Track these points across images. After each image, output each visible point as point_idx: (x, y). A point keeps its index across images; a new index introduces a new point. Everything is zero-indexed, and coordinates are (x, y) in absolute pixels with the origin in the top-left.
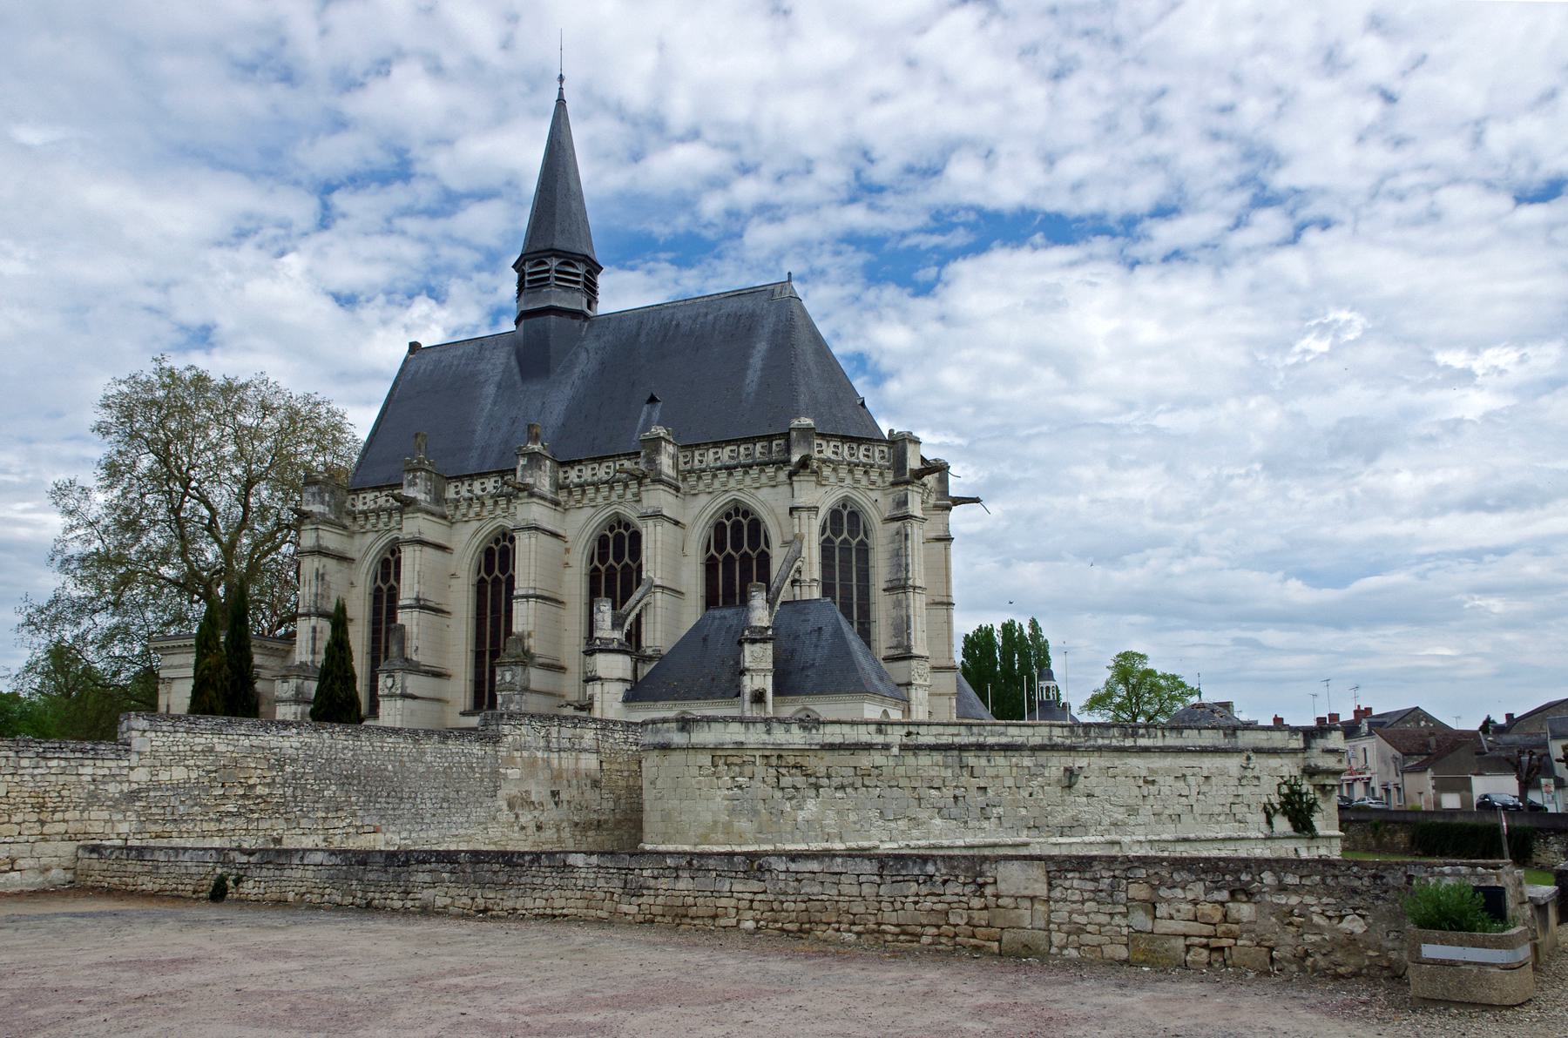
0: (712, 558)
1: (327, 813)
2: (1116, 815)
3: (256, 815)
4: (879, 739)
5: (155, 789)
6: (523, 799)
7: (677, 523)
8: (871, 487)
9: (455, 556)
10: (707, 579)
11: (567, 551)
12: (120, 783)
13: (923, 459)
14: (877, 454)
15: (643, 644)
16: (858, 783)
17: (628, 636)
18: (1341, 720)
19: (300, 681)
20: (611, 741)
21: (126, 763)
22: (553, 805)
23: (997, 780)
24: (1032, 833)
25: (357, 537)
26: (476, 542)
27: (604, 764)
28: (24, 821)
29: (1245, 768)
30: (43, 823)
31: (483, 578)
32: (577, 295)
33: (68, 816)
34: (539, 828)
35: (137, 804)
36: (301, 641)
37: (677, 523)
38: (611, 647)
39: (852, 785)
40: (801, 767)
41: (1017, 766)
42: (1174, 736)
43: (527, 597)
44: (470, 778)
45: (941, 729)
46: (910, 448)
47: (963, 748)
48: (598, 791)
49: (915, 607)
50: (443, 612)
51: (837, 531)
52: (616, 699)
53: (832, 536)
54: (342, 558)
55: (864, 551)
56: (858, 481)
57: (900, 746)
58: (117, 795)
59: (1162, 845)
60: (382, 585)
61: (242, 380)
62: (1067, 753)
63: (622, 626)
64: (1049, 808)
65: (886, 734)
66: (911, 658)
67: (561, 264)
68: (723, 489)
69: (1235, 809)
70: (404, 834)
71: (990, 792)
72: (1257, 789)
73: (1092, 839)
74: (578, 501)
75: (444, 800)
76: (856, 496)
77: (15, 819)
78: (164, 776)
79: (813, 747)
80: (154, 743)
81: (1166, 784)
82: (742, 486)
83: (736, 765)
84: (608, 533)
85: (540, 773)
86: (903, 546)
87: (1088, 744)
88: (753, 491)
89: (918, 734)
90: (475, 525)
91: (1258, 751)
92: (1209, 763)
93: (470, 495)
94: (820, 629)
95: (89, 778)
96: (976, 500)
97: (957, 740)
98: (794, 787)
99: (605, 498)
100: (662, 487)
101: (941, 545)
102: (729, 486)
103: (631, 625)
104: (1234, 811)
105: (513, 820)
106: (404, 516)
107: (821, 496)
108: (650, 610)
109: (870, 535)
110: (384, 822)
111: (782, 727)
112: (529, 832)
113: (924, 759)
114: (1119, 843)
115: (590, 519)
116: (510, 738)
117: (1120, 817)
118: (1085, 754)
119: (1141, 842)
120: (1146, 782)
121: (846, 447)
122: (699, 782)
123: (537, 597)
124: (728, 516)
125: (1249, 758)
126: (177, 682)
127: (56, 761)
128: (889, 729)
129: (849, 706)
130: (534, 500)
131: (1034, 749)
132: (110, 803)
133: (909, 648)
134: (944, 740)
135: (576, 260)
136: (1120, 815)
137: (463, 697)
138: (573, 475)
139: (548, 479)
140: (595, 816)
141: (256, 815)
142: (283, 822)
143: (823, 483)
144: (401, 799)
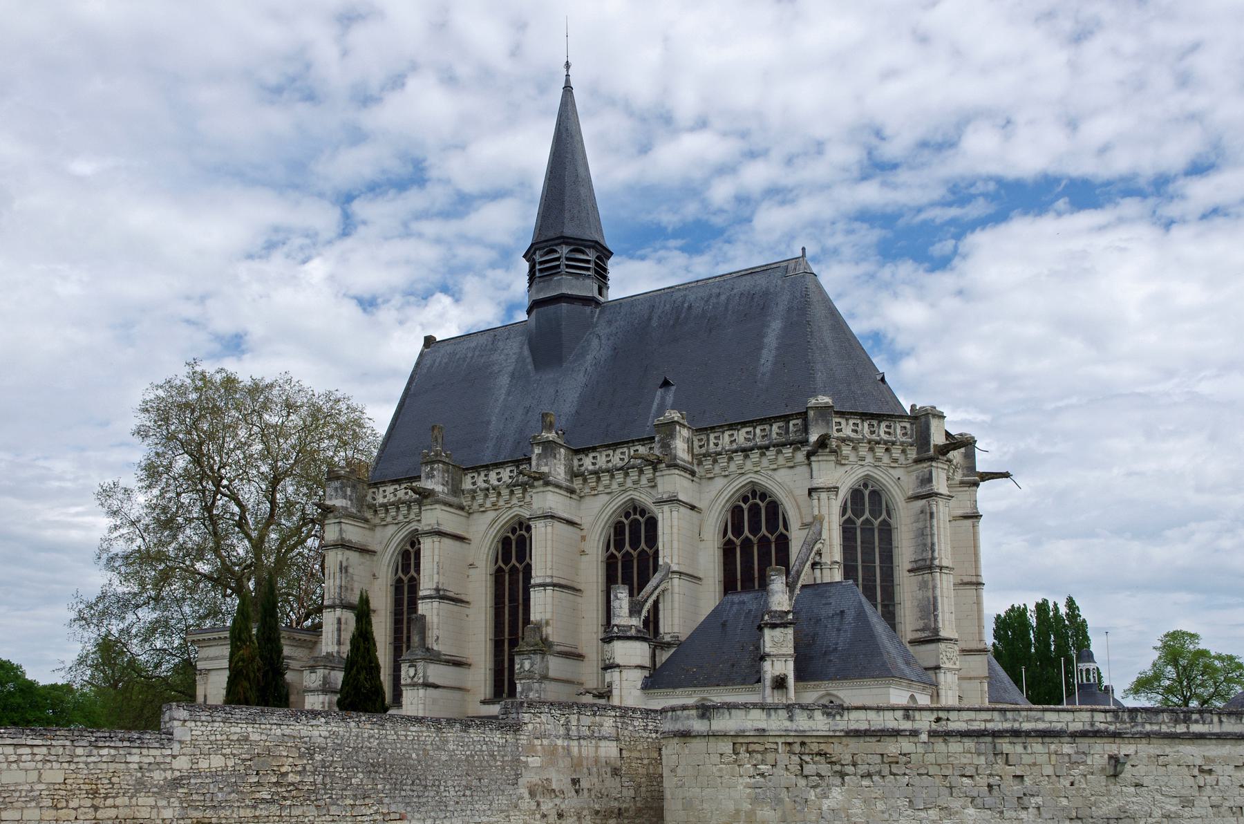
0: (729, 542)
1: (355, 801)
2: (1168, 807)
3: (289, 802)
4: (907, 725)
5: (195, 777)
6: (544, 787)
7: (693, 508)
8: (893, 465)
10: (725, 564)
11: (583, 538)
12: (165, 770)
13: (948, 435)
14: (898, 431)
15: (661, 630)
16: (886, 771)
17: (646, 623)
19: (327, 671)
21: (169, 752)
22: (573, 793)
26: (493, 532)
27: (624, 752)
28: (79, 807)
30: (96, 808)
31: (500, 567)
32: (588, 281)
33: (119, 801)
35: (180, 790)
37: (693, 508)
38: (629, 634)
39: (879, 773)
40: (825, 754)
42: (1233, 721)
43: (544, 585)
45: (972, 715)
46: (934, 423)
47: (996, 734)
48: (618, 779)
49: (942, 588)
50: (462, 601)
51: (858, 512)
52: (635, 687)
54: (364, 551)
55: (887, 531)
57: (929, 732)
58: (162, 782)
60: (503, 566)
61: (268, 381)
62: (1111, 740)
63: (640, 612)
64: (1093, 799)
65: (914, 720)
66: (939, 640)
67: (571, 251)
71: (1028, 781)
74: (593, 489)
75: (466, 787)
76: (878, 474)
77: (72, 805)
78: (203, 764)
79: (838, 734)
83: (758, 752)
84: (623, 519)
85: (560, 762)
86: (928, 525)
89: (948, 719)
90: (491, 515)
94: (842, 612)
96: (1006, 475)
97: (990, 726)
98: (819, 775)
99: (620, 485)
100: (677, 472)
101: (969, 522)
102: (746, 468)
105: (535, 808)
106: (423, 508)
108: (668, 596)
110: (409, 809)
111: (805, 713)
113: (955, 746)
115: (605, 506)
117: (1173, 809)
118: (1132, 741)
120: (1201, 771)
121: (866, 425)
122: (720, 770)
123: (554, 585)
124: (745, 499)
126: (213, 673)
128: (917, 714)
130: (550, 488)
131: (1075, 735)
132: (156, 790)
134: (976, 726)
135: (585, 247)
138: (588, 462)
139: (563, 468)
140: (616, 804)
144: (426, 787)
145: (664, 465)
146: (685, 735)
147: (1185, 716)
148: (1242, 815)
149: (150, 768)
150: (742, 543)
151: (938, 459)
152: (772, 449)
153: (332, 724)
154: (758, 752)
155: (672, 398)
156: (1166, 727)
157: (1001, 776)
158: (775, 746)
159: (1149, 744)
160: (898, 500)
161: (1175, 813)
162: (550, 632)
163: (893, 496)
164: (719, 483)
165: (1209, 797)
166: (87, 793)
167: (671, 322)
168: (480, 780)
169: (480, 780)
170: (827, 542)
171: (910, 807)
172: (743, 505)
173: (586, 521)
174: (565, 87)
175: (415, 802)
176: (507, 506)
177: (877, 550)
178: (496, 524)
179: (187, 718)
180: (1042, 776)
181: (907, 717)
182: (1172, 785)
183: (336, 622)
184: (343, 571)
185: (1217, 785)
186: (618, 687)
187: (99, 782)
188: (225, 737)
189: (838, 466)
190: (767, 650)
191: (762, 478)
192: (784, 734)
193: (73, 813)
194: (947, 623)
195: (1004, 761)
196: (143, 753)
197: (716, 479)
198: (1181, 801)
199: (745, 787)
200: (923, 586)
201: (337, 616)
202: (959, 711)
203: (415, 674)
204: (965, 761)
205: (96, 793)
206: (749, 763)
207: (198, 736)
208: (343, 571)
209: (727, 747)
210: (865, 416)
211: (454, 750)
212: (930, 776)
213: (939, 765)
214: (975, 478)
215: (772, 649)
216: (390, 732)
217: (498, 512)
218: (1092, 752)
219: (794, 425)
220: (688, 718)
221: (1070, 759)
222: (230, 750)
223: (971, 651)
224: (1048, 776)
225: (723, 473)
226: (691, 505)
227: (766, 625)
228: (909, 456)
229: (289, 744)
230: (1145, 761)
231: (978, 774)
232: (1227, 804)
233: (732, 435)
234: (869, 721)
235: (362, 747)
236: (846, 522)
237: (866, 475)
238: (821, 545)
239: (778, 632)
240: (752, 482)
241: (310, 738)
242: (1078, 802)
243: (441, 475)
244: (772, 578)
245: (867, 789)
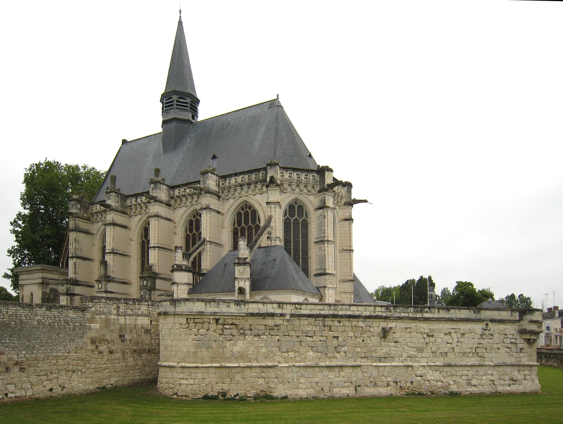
2: (410, 352)
4: (279, 311)
6: (101, 338)
7: (219, 212)
8: (308, 193)
9: (132, 231)
10: (234, 238)
11: (176, 227)
15: (202, 268)
17: (194, 263)
18: (559, 309)
19: (68, 286)
22: (120, 341)
23: (344, 333)
24: (362, 360)
25: (95, 224)
26: (140, 224)
27: (153, 322)
29: (485, 330)
31: (144, 240)
34: (111, 352)
36: (70, 269)
37: (219, 212)
40: (236, 325)
41: (355, 326)
42: (445, 312)
43: (154, 247)
44: (66, 328)
45: (313, 307)
46: (327, 173)
47: (325, 316)
48: (149, 335)
49: (328, 251)
51: (292, 215)
52: (185, 293)
54: (87, 232)
55: (305, 224)
56: (302, 191)
57: (290, 315)
59: (436, 368)
60: (238, 227)
62: (384, 320)
64: (373, 348)
65: (283, 309)
66: (325, 274)
68: (239, 196)
69: (478, 350)
71: (340, 339)
72: (491, 341)
73: (397, 364)
74: (179, 204)
76: (301, 197)
79: (241, 314)
81: (440, 338)
82: (247, 194)
83: (199, 323)
84: (193, 218)
86: (323, 221)
87: (395, 315)
88: (306, 195)
89: (301, 309)
90: (139, 217)
91: (493, 321)
92: (463, 327)
93: (136, 203)
94: (275, 259)
96: (366, 201)
97: (322, 312)
98: (231, 335)
99: (190, 203)
100: (209, 195)
101: (347, 222)
102: (242, 194)
104: (477, 351)
106: (107, 213)
107: (286, 199)
108: (205, 252)
109: (308, 216)
111: (225, 304)
112: (105, 354)
113: (305, 321)
114: (412, 366)
116: (93, 309)
117: (413, 353)
118: (394, 321)
119: (424, 366)
120: (428, 335)
121: (295, 174)
122: (180, 332)
123: (159, 247)
125: (487, 325)
126: (25, 286)
128: (284, 306)
129: (285, 296)
130: (157, 203)
133: (325, 270)
135: (185, 96)
136: (412, 352)
137: (136, 293)
138: (177, 192)
139: (164, 194)
143: (284, 191)
145: (204, 192)
146: (166, 314)
147: (421, 310)
148: (447, 357)
150: (241, 229)
151: (328, 190)
154: (199, 323)
155: (216, 164)
156: (411, 315)
157: (327, 337)
158: (209, 320)
159: (403, 322)
160: (311, 210)
161: (414, 355)
163: (308, 208)
164: (231, 201)
165: (431, 348)
167: (220, 130)
168: (58, 335)
169: (58, 335)
170: (274, 228)
171: (279, 351)
172: (242, 211)
173: (177, 219)
174: (179, 22)
176: (145, 213)
177: (292, 229)
178: (141, 221)
180: (348, 337)
182: (413, 342)
183: (74, 264)
185: (435, 342)
186: (176, 293)
189: (282, 194)
190: (236, 276)
191: (249, 199)
194: (330, 266)
195: (329, 329)
197: (230, 199)
198: (417, 349)
199: (192, 340)
200: (321, 249)
201: (74, 261)
202: (306, 304)
203: (102, 287)
204: (308, 329)
206: (195, 328)
208: (77, 242)
209: (184, 321)
210: (294, 169)
212: (290, 336)
213: (295, 331)
214: (352, 203)
215: (238, 276)
216: (55, 312)
217: (142, 215)
218: (373, 326)
219: (262, 174)
221: (362, 329)
224: (351, 337)
225: (233, 197)
226: (217, 211)
227: (236, 263)
228: (316, 189)
230: (400, 331)
231: (315, 336)
232: (439, 351)
234: (259, 309)
236: (286, 219)
237: (295, 198)
238: (271, 229)
239: (241, 268)
240: (245, 200)
242: (366, 350)
243: (114, 198)
245: (257, 342)
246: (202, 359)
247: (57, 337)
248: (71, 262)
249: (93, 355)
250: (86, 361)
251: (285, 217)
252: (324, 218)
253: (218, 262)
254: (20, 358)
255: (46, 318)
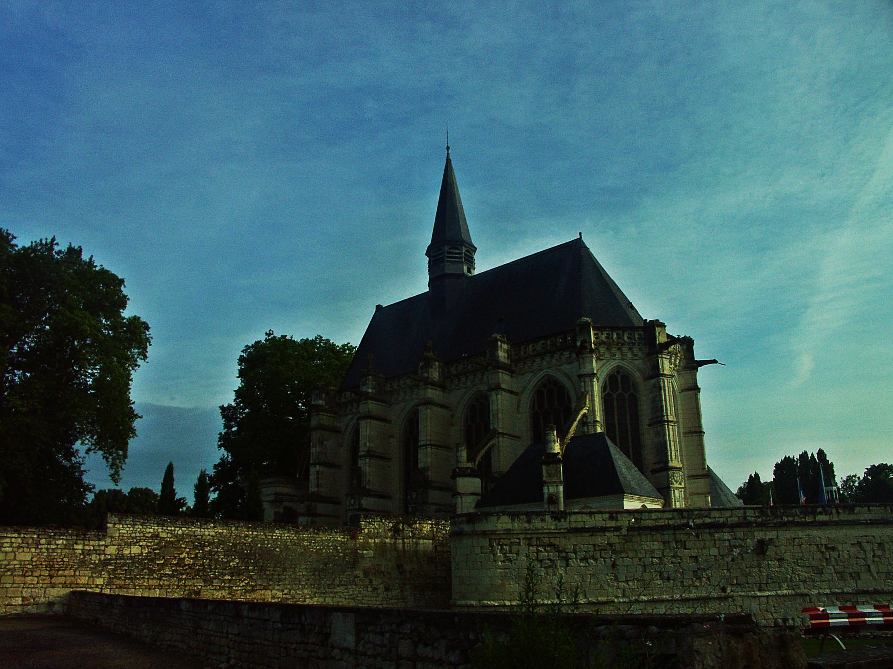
1: (231, 577)
3: (184, 577)
4: (612, 524)
5: (120, 559)
8: (635, 358)
12: (99, 554)
13: (669, 336)
14: (636, 336)
16: (598, 556)
20: (443, 532)
21: (103, 543)
28: (40, 575)
30: (51, 577)
33: (67, 573)
35: (109, 567)
39: (593, 558)
43: (425, 446)
46: (658, 329)
53: (610, 392)
57: (628, 528)
58: (97, 562)
65: (617, 520)
67: (450, 249)
70: (286, 591)
76: (625, 364)
77: (36, 574)
78: (126, 552)
80: (121, 531)
89: (641, 519)
90: (402, 405)
95: (81, 552)
96: (715, 361)
103: (481, 458)
105: (367, 583)
110: (271, 583)
127: (61, 541)
131: (733, 526)
132: (92, 566)
139: (437, 374)
141: (184, 577)
142: (202, 581)
143: (601, 358)
145: (491, 367)
149: (90, 552)
152: (557, 352)
153: (218, 528)
158: (518, 541)
162: (431, 475)
166: (46, 567)
175: (276, 579)
179: (117, 522)
181: (611, 518)
184: (320, 443)
187: (55, 560)
188: (142, 535)
192: (524, 532)
193: (36, 579)
195: (683, 547)
196: (86, 543)
205: (52, 567)
207: (124, 533)
208: (320, 443)
209: (486, 543)
211: (307, 545)
213: (636, 551)
220: (461, 523)
222: (145, 543)
223: (698, 476)
225: (530, 370)
229: (187, 540)
231: (664, 556)
233: (534, 346)
234: (584, 522)
235: (239, 543)
237: (617, 366)
240: (547, 374)
241: (202, 536)
244: (547, 432)
246: (511, 595)
247: (325, 567)
248: (313, 470)
249: (365, 592)
250: (359, 600)
251: (605, 394)
252: (660, 390)
253: (514, 461)
254: (284, 594)
255: (313, 543)
